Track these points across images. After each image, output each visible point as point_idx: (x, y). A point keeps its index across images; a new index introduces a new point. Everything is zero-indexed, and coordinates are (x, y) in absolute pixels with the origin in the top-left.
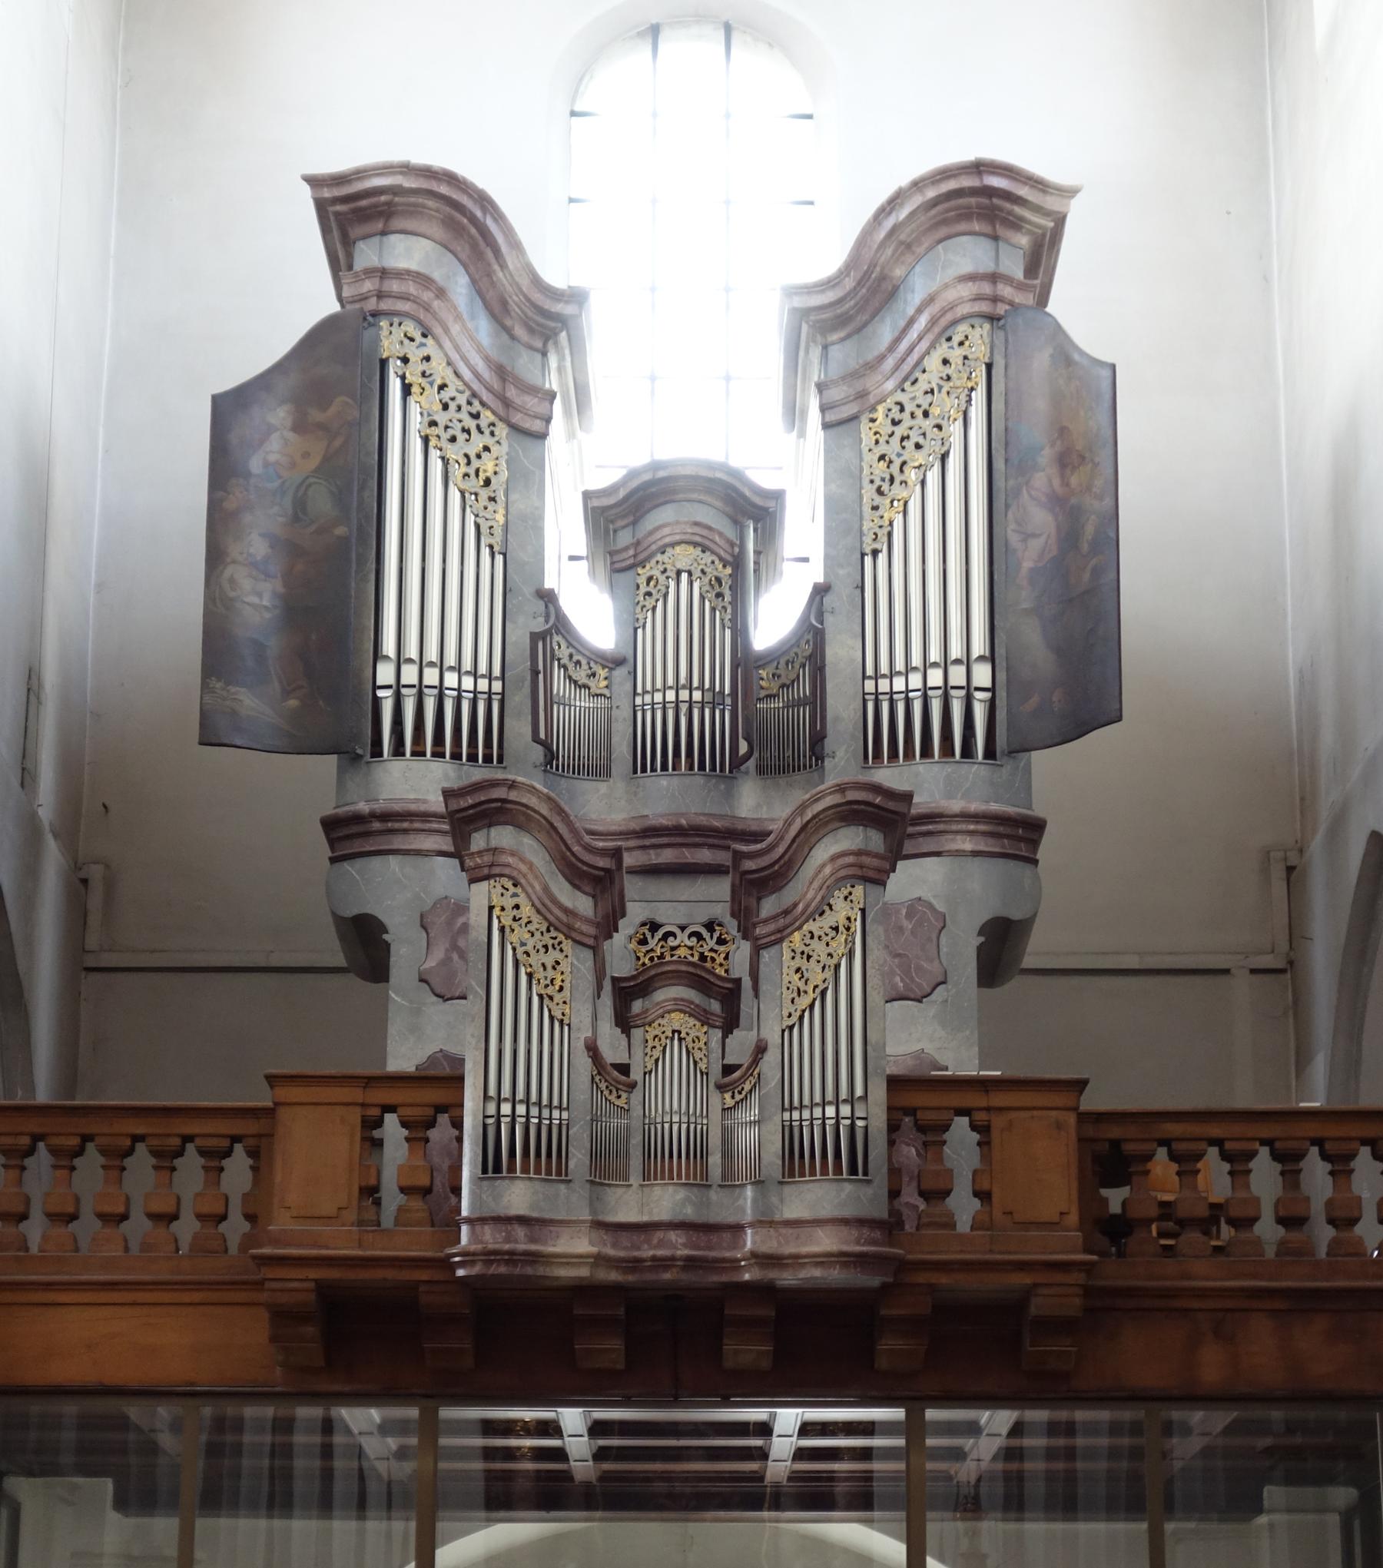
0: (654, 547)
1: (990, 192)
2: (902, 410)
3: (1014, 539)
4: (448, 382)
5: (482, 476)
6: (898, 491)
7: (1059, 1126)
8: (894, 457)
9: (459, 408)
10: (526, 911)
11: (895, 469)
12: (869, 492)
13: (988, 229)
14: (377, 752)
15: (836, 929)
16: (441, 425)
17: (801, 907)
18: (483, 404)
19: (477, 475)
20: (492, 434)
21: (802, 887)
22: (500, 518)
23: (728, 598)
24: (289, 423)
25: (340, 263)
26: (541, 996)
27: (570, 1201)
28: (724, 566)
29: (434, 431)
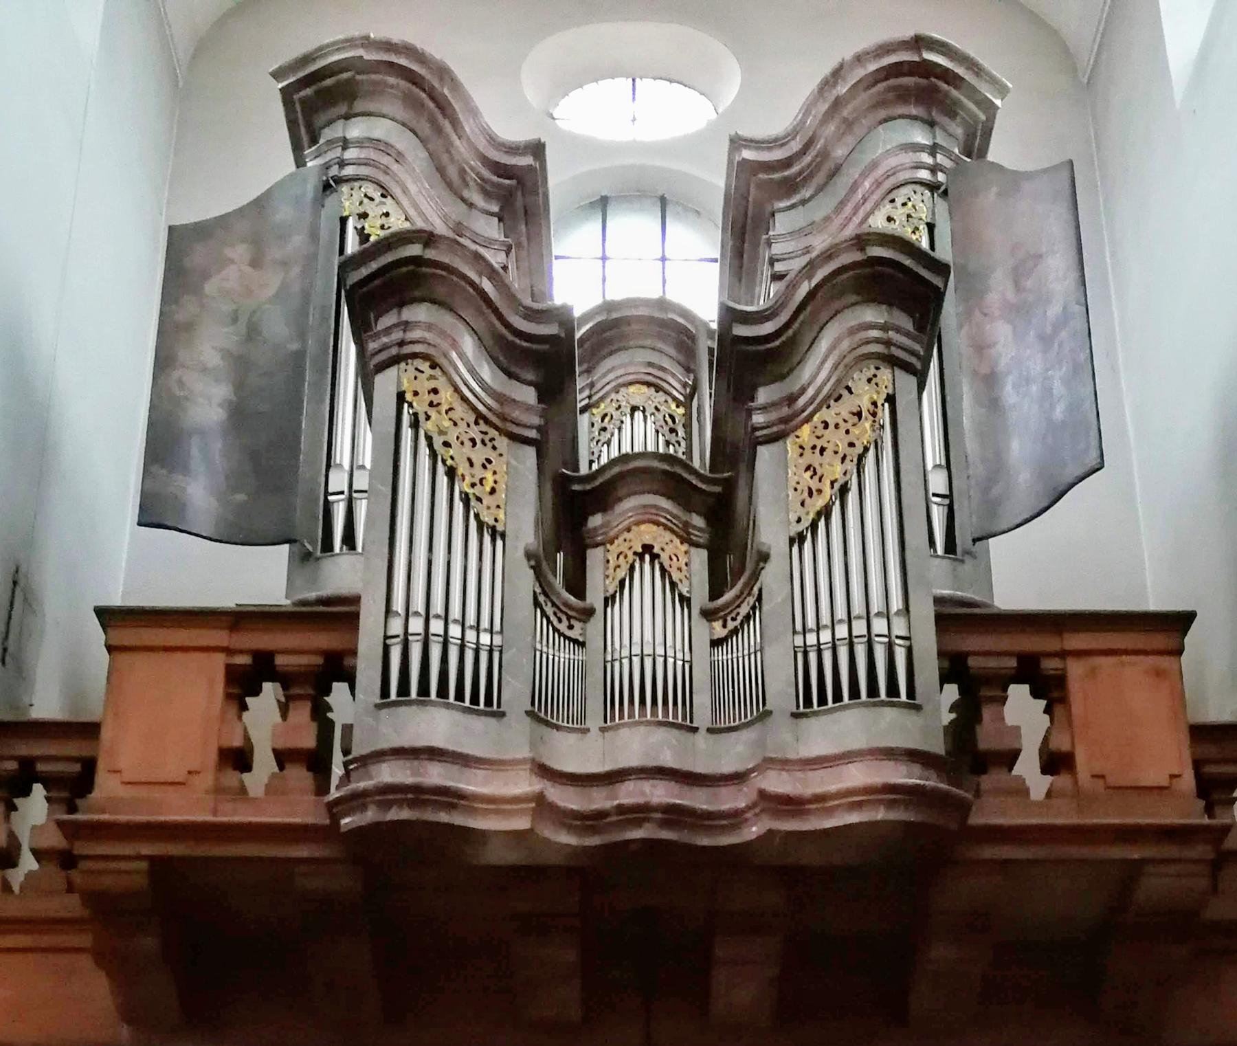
0: (608, 388)
1: (927, 69)
14: (327, 546)
17: (810, 392)
21: (816, 368)
26: (466, 499)
27: (511, 737)
28: (678, 407)
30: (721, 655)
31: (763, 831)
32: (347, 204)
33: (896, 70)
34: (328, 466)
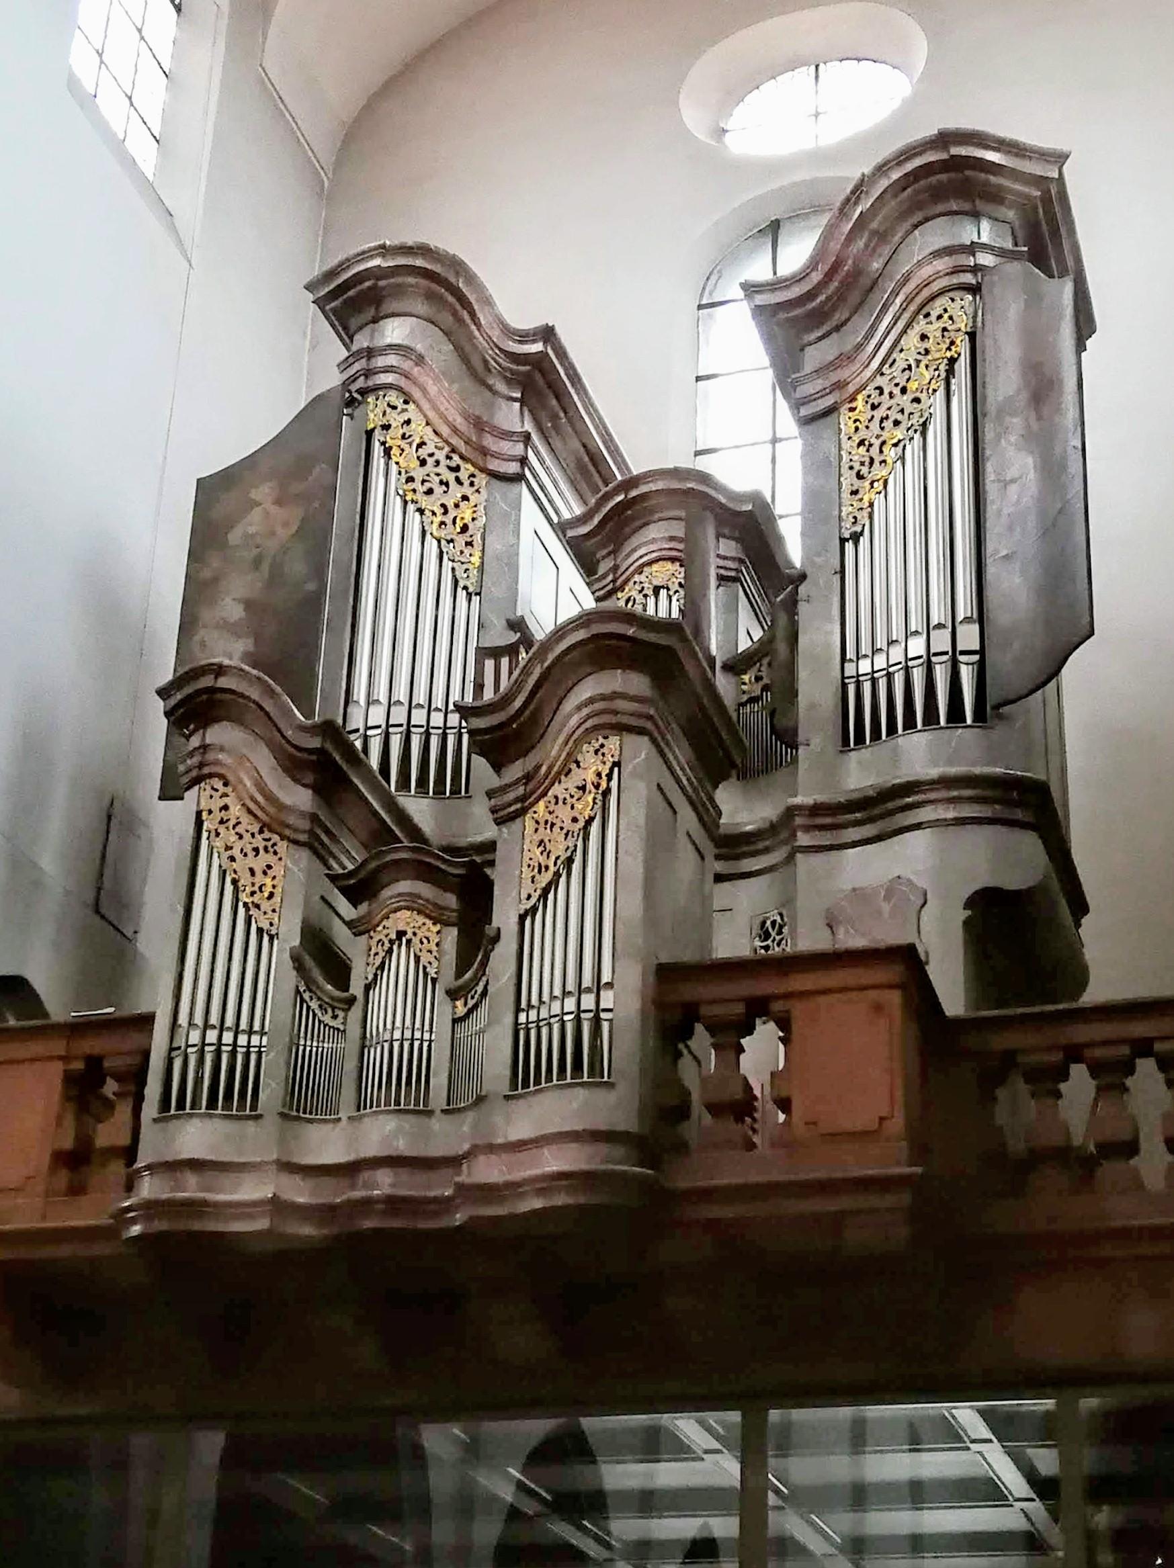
0: (632, 569)
4: (426, 439)
5: (459, 524)
6: (879, 472)
7: (878, 1008)
8: (873, 440)
9: (438, 463)
10: (236, 810)
11: (875, 451)
12: (848, 480)
13: (967, 206)
15: (583, 788)
16: (418, 479)
17: (544, 769)
18: (462, 457)
19: (454, 522)
20: (472, 484)
22: (476, 560)
26: (245, 904)
27: (255, 1141)
31: (465, 1218)
32: (371, 416)
33: (927, 170)
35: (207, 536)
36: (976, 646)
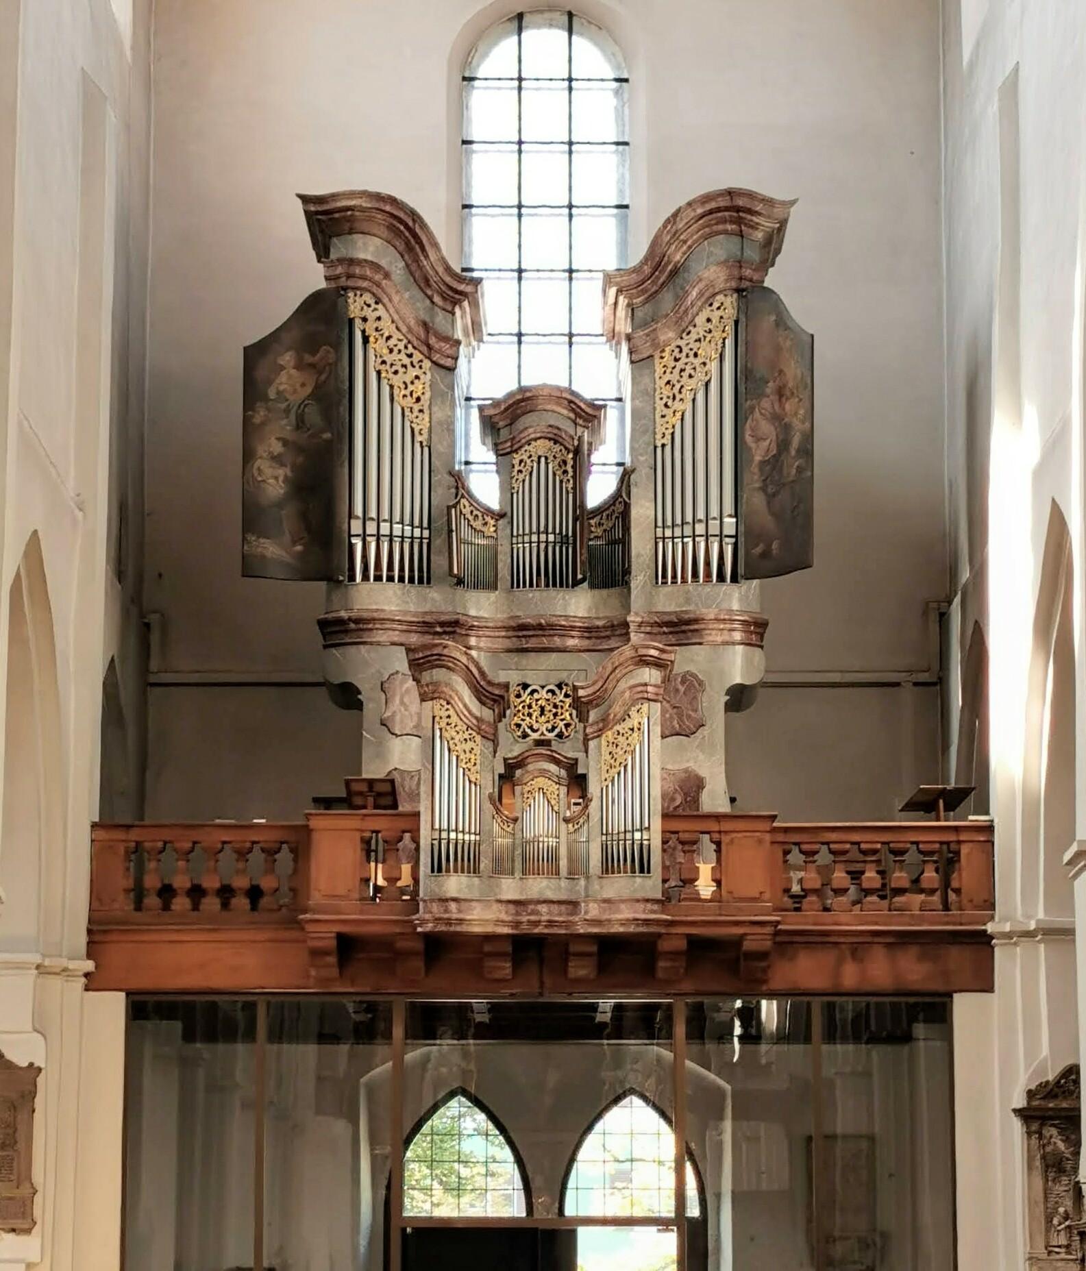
1: (738, 209)
2: (681, 351)
3: (748, 439)
5: (415, 396)
6: (677, 405)
7: (760, 841)
9: (400, 351)
11: (676, 390)
12: (659, 405)
14: (352, 578)
15: (632, 730)
18: (414, 348)
23: (571, 474)
24: (292, 364)
25: (322, 250)
29: (383, 367)
30: (573, 837)
34: (350, 518)
35: (253, 391)
36: (733, 533)
